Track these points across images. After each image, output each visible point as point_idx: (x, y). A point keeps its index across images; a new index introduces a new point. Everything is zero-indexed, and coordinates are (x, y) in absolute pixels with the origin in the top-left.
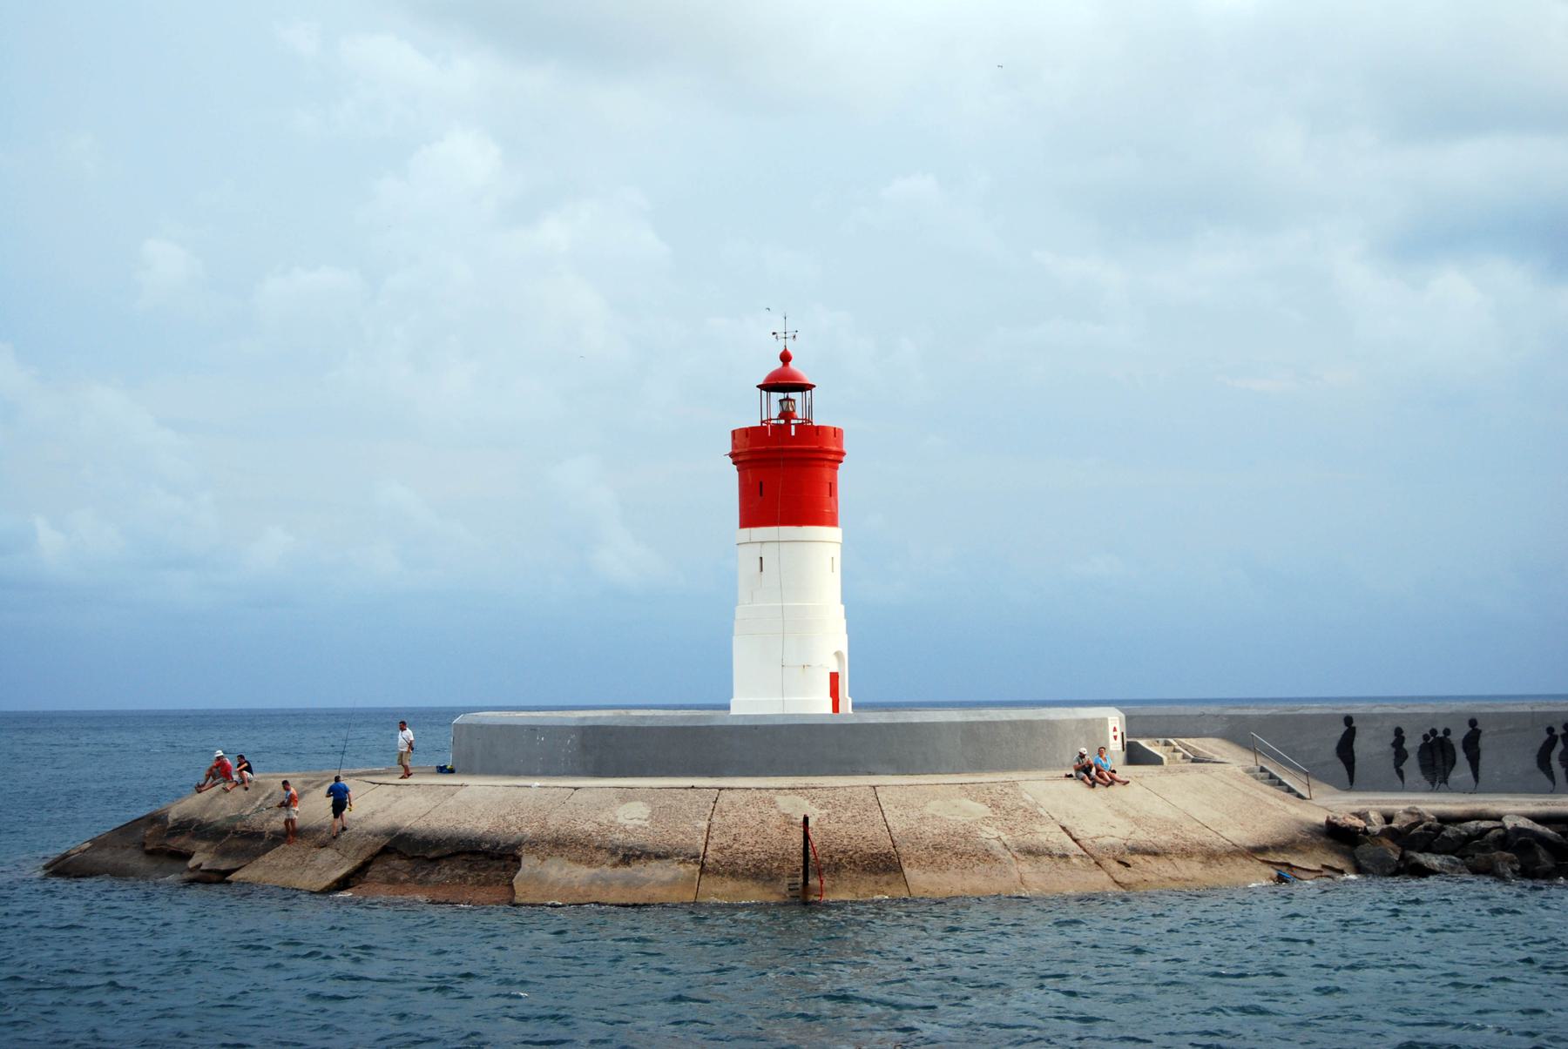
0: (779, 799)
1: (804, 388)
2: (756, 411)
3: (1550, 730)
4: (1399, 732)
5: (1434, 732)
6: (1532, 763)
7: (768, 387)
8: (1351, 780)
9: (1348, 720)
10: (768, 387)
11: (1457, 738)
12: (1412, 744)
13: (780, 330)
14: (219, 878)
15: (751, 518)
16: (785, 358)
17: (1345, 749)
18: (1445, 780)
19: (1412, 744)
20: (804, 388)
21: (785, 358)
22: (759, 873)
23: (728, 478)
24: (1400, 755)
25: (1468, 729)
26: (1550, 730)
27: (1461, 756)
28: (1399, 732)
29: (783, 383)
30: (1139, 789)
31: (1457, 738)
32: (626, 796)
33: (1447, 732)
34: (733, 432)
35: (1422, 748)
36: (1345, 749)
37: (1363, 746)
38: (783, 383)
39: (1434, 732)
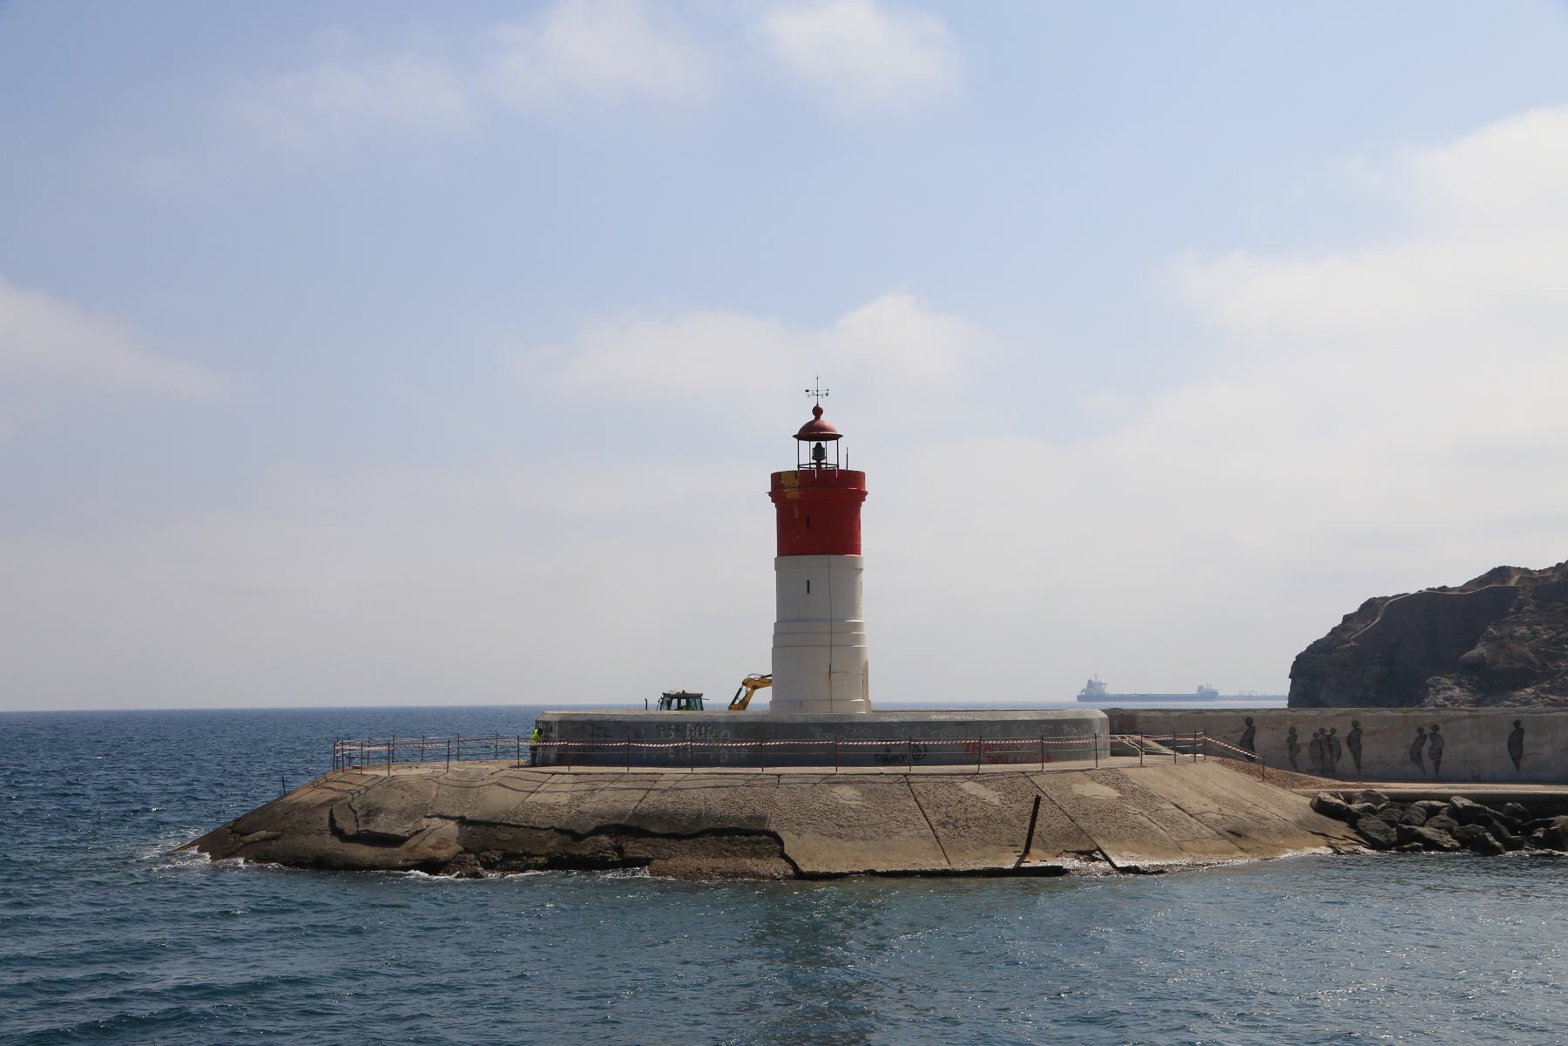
1: (836, 437)
2: (798, 456)
3: (1420, 730)
5: (1322, 731)
7: (802, 436)
9: (1249, 721)
10: (802, 436)
12: (1305, 738)
13: (813, 388)
14: (476, 875)
15: (776, 477)
16: (818, 411)
19: (1305, 738)
20: (836, 437)
21: (818, 411)
23: (767, 516)
25: (1350, 729)
26: (1420, 730)
27: (1346, 750)
29: (815, 432)
32: (831, 781)
33: (1333, 731)
34: (776, 477)
35: (1312, 743)
36: (1248, 742)
37: (1262, 738)
38: (815, 432)
39: (1322, 731)
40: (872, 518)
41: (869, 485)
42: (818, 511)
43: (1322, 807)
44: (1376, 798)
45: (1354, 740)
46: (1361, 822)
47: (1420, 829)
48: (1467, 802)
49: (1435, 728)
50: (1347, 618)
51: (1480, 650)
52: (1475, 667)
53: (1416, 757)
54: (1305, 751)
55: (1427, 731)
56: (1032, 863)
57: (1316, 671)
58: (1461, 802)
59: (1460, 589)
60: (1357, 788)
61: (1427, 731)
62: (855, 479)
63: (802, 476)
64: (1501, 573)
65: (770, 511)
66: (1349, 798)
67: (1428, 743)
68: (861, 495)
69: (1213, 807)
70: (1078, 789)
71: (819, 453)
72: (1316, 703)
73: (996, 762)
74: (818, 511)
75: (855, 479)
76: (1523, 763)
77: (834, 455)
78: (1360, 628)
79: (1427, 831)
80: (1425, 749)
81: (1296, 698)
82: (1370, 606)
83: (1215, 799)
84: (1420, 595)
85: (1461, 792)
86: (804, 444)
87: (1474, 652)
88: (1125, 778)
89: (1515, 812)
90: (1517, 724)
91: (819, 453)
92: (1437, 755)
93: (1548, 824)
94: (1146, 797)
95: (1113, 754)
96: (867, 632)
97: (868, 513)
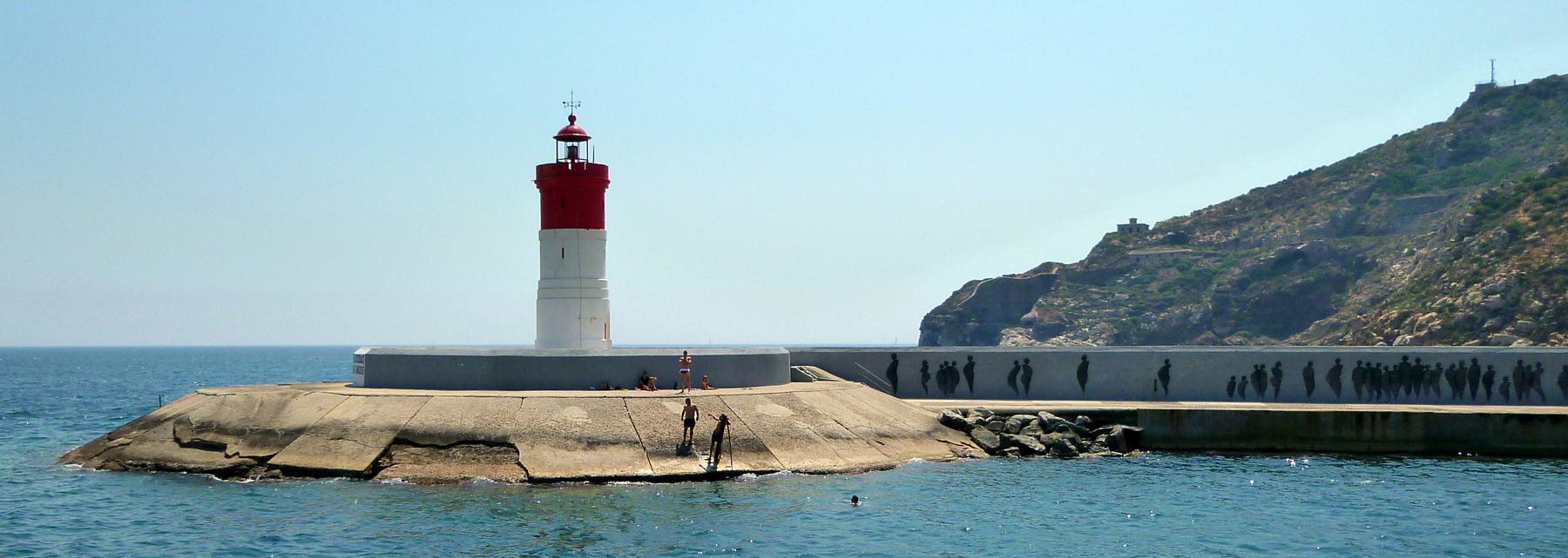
0: (666, 403)
1: (586, 139)
2: (554, 153)
4: (925, 364)
6: (1004, 382)
7: (558, 138)
8: (1310, 364)
9: (894, 356)
10: (558, 138)
11: (960, 367)
12: (933, 370)
15: (540, 169)
16: (572, 119)
17: (892, 373)
18: (952, 391)
19: (933, 370)
20: (586, 139)
21: (572, 119)
22: (888, 371)
24: (925, 376)
25: (714, 424)
27: (962, 377)
28: (925, 364)
29: (569, 135)
30: (642, 432)
31: (960, 367)
32: (564, 403)
36: (892, 373)
40: (613, 200)
41: (611, 175)
42: (572, 195)
43: (947, 422)
44: (986, 414)
45: (969, 369)
46: (974, 432)
47: (1016, 437)
48: (1051, 416)
49: (1027, 361)
50: (955, 293)
51: (1033, 314)
52: (1029, 324)
53: (1012, 379)
54: (933, 377)
55: (1021, 363)
56: (720, 468)
57: (932, 326)
58: (1045, 416)
59: (1024, 275)
60: (972, 405)
61: (1021, 363)
62: (602, 170)
63: (559, 166)
64: (1047, 266)
65: (535, 196)
66: (965, 414)
67: (1021, 372)
68: (605, 183)
69: (865, 422)
70: (760, 409)
71: (573, 153)
72: (934, 344)
73: (1128, 412)
74: (572, 195)
75: (602, 170)
76: (1170, 386)
77: (584, 153)
78: (966, 298)
79: (1021, 438)
80: (1019, 377)
81: (925, 341)
82: (969, 286)
83: (867, 416)
84: (999, 279)
85: (1046, 407)
86: (561, 143)
87: (1029, 315)
88: (798, 401)
89: (1085, 423)
90: (1084, 357)
91: (573, 153)
92: (1027, 379)
93: (1107, 432)
94: (812, 414)
95: (793, 380)
96: (609, 287)
97: (610, 197)
